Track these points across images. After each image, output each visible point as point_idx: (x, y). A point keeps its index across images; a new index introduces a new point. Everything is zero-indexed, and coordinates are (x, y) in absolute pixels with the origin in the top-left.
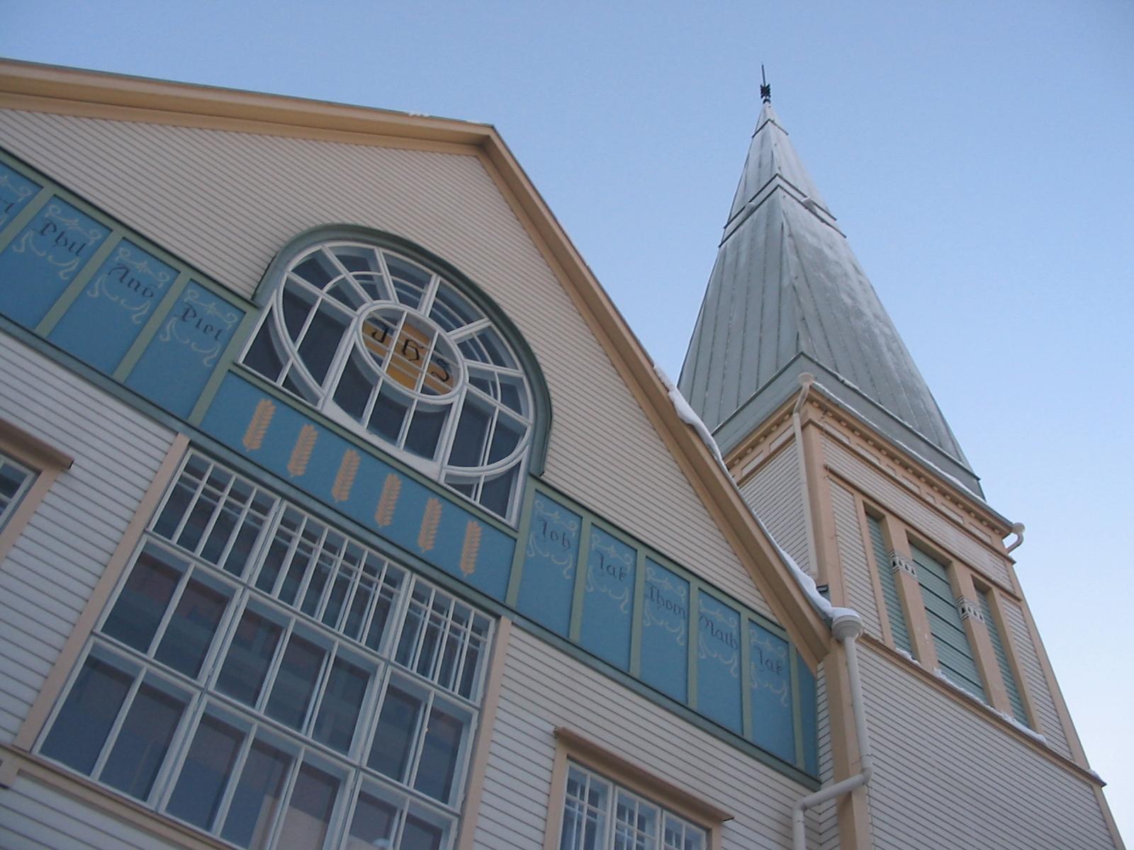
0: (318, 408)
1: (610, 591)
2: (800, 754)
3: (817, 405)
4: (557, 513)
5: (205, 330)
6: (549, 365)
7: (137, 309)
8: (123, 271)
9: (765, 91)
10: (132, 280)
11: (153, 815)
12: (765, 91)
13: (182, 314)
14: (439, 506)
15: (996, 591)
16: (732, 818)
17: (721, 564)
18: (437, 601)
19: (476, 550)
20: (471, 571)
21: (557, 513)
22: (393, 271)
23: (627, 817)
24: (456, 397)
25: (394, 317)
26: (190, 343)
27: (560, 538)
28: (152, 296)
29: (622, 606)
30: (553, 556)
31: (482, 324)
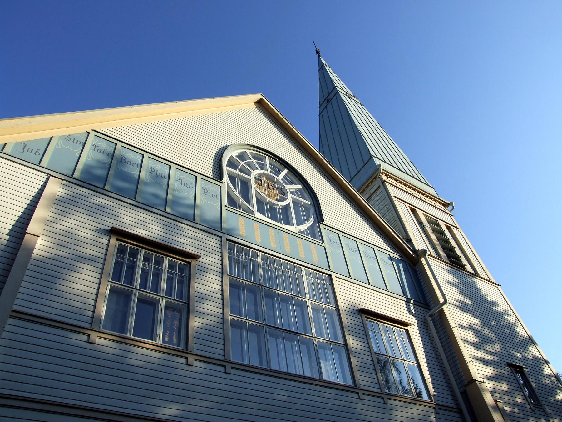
0: (255, 216)
1: (336, 250)
2: (421, 299)
3: (442, 204)
4: (211, 186)
5: (133, 165)
6: (311, 182)
7: (78, 150)
8: (180, 181)
9: (318, 52)
10: (78, 141)
11: (270, 370)
12: (318, 52)
13: (94, 149)
14: (243, 219)
15: (452, 227)
16: (413, 325)
17: (453, 271)
18: (229, 247)
19: (244, 227)
20: (290, 252)
21: (159, 165)
22: (270, 164)
23: (242, 289)
24: (289, 201)
25: (261, 175)
26: (211, 202)
27: (336, 243)
28: (192, 188)
29: (217, 207)
30: (336, 250)
31: (286, 171)
